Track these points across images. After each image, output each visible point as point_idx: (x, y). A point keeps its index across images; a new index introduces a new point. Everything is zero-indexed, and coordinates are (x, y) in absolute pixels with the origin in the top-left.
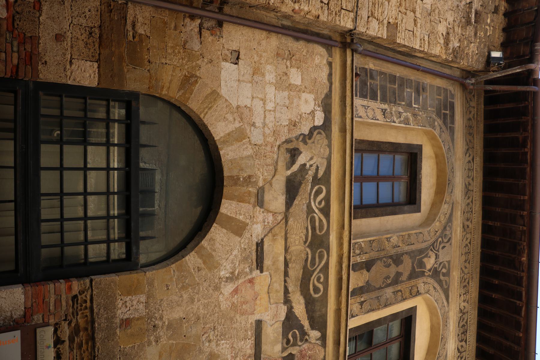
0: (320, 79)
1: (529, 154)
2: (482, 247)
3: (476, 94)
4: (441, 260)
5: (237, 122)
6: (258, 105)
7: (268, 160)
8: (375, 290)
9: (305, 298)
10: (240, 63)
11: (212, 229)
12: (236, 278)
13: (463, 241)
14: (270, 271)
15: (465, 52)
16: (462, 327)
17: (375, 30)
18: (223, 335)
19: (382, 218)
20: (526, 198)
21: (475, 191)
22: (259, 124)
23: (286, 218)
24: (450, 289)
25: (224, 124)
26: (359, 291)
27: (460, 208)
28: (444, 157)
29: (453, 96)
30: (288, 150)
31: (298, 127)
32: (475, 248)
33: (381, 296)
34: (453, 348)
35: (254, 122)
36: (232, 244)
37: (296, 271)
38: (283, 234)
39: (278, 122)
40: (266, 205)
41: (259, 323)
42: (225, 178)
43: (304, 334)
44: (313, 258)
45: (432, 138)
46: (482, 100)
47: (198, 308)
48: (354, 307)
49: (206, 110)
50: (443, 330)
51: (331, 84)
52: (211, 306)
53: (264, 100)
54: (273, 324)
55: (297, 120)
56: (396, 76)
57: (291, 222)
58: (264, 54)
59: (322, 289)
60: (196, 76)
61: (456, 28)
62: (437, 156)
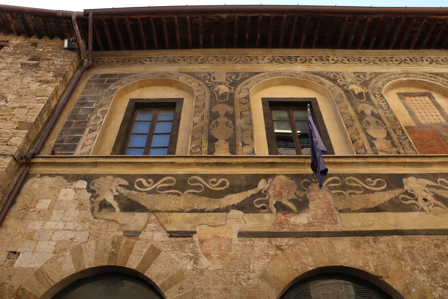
0: (52, 183)
1: (142, 16)
2: (222, 47)
3: (100, 58)
4: (224, 80)
5: (66, 254)
6: (58, 236)
7: (103, 227)
8: (235, 134)
9: (227, 194)
10: (19, 251)
11: (149, 276)
12: (196, 255)
13: (213, 63)
14: (196, 225)
15: (59, 67)
16: (285, 60)
17: (18, 140)
18: (245, 267)
19: (180, 130)
20: (176, 17)
21: (175, 56)
22: (71, 235)
23: (155, 212)
24: (251, 71)
25: (64, 265)
26: (233, 148)
27: (185, 67)
28: (141, 81)
29: (96, 76)
30: (100, 210)
31: (84, 201)
32: (221, 53)
33: (242, 128)
34: (301, 66)
35: (70, 239)
36: (166, 259)
37: (202, 203)
38: (167, 214)
39: (75, 219)
40: (139, 229)
41: (241, 234)
42: (109, 264)
43: (260, 194)
44: (195, 188)
45: (125, 91)
46: (106, 52)
47: (216, 289)
48: (246, 150)
49: (49, 280)
50: (284, 76)
51: (58, 175)
52: (217, 278)
53: (55, 230)
54: (245, 222)
55: (78, 203)
56: (67, 122)
57: (158, 208)
58: (18, 231)
59: (223, 179)
60: (18, 290)
61: (38, 75)
62: (141, 87)
